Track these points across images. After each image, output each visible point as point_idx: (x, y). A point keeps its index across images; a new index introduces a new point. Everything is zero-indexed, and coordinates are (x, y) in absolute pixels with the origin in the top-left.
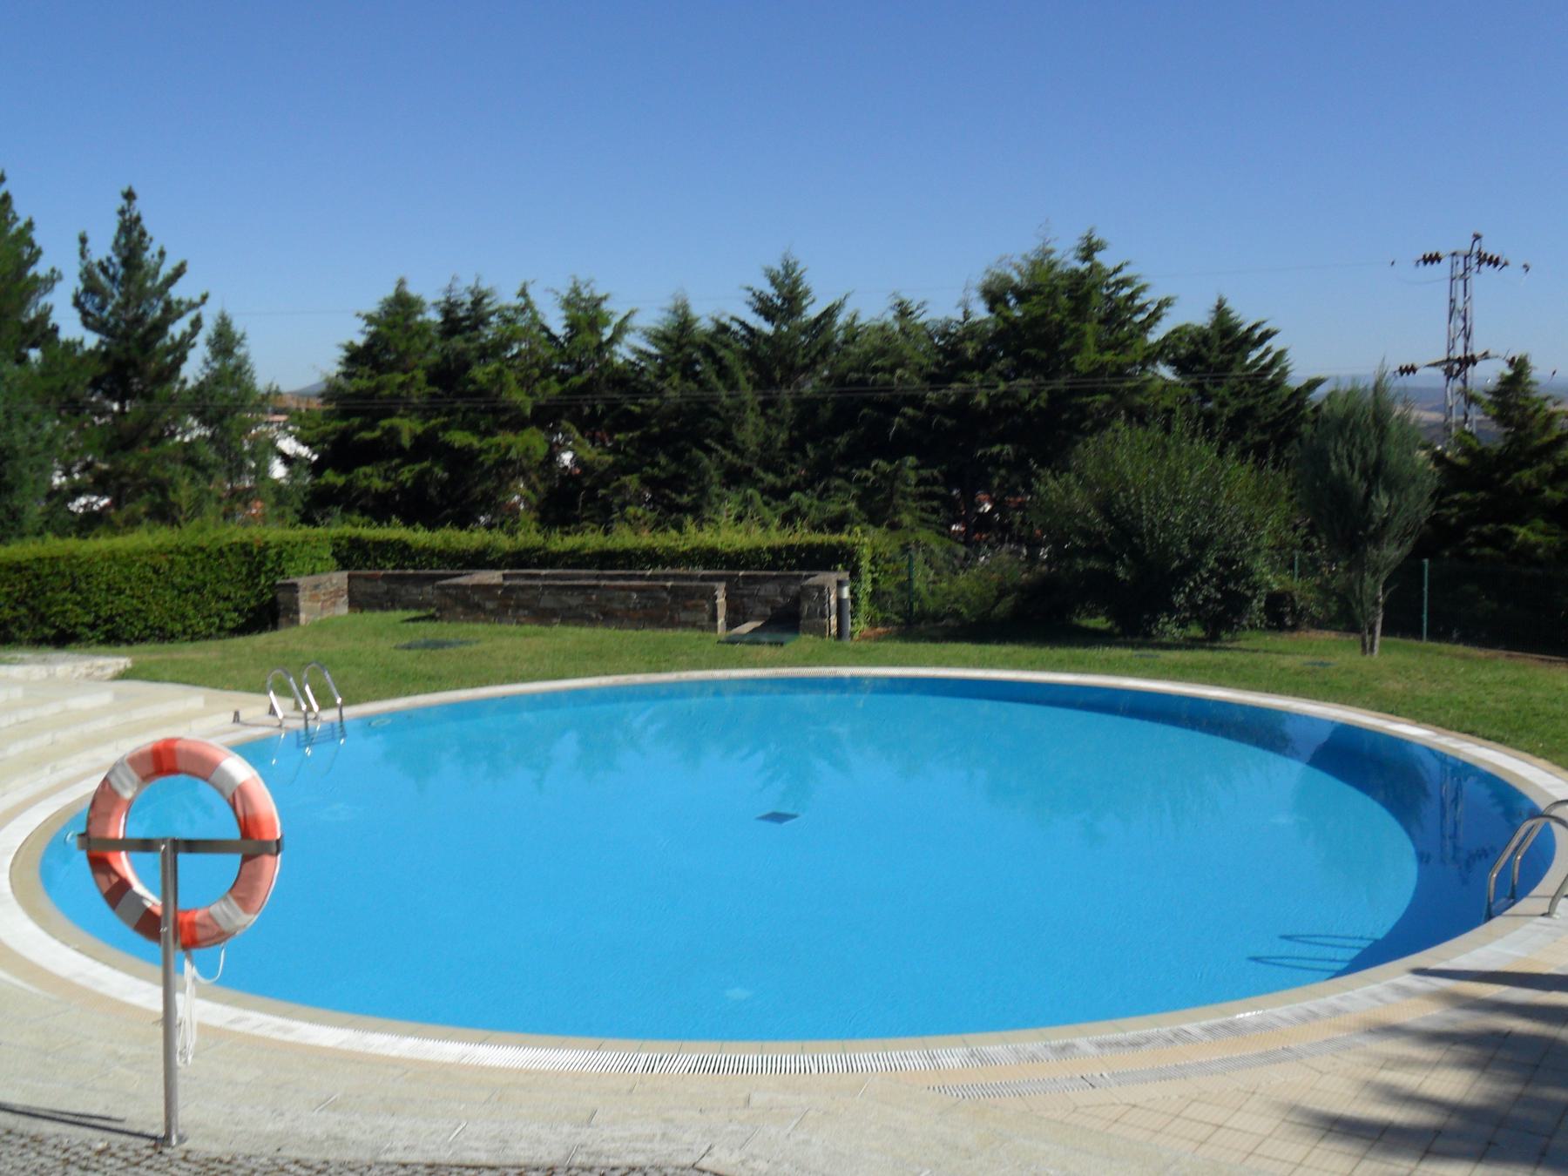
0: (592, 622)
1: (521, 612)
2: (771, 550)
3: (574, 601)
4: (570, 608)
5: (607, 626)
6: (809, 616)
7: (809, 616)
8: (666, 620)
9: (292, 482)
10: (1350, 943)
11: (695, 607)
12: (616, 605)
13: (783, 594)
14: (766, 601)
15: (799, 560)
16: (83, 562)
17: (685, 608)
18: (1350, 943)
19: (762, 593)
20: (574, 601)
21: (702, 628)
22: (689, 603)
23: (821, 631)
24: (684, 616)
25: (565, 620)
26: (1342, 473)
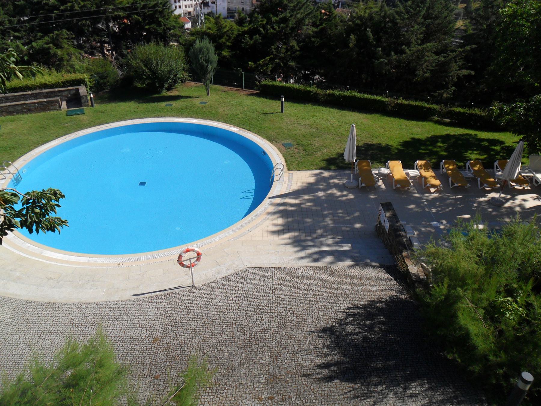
0: (26, 113)
1: (3, 113)
2: (62, 82)
3: (19, 108)
4: (18, 110)
5: (30, 113)
6: (84, 103)
7: (84, 103)
8: (47, 109)
9: (416, 281)
10: (251, 191)
11: (55, 105)
12: (32, 108)
13: (69, 94)
14: (65, 96)
15: (70, 84)
16: (404, 260)
17: (52, 106)
18: (251, 191)
19: (64, 94)
20: (19, 108)
21: (57, 110)
22: (53, 104)
23: (88, 106)
24: (52, 108)
25: (17, 113)
26: (202, 62)
